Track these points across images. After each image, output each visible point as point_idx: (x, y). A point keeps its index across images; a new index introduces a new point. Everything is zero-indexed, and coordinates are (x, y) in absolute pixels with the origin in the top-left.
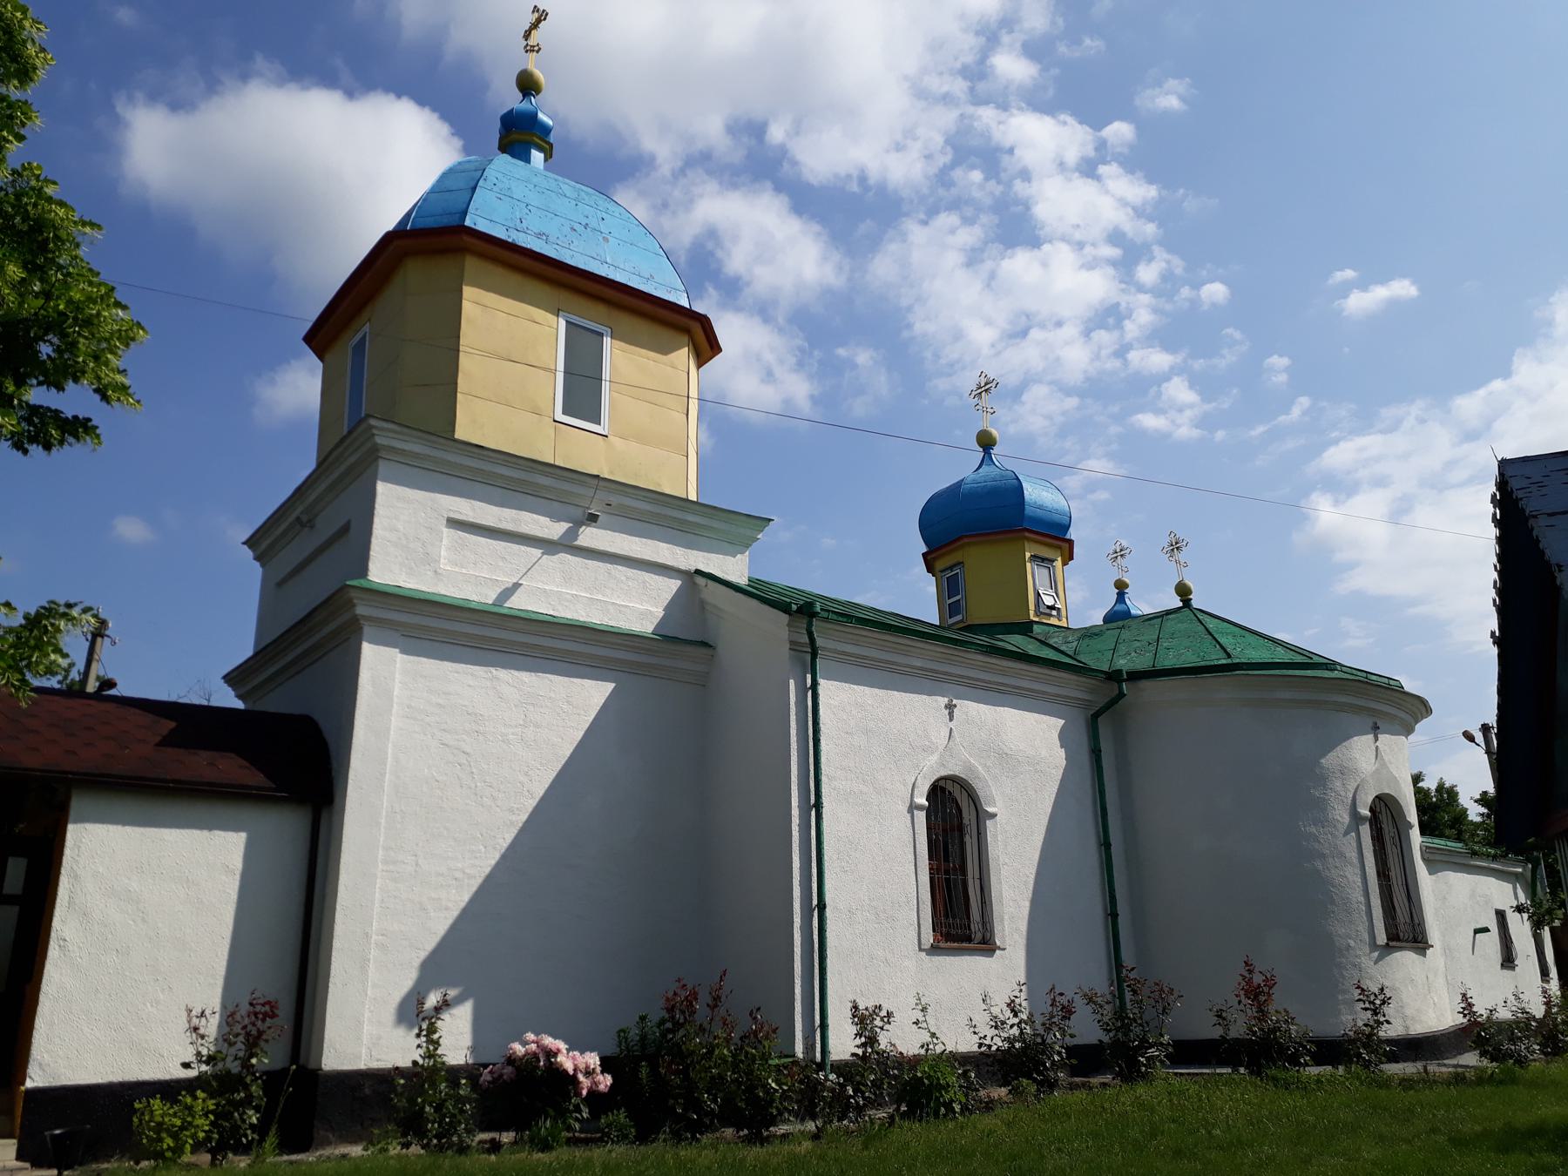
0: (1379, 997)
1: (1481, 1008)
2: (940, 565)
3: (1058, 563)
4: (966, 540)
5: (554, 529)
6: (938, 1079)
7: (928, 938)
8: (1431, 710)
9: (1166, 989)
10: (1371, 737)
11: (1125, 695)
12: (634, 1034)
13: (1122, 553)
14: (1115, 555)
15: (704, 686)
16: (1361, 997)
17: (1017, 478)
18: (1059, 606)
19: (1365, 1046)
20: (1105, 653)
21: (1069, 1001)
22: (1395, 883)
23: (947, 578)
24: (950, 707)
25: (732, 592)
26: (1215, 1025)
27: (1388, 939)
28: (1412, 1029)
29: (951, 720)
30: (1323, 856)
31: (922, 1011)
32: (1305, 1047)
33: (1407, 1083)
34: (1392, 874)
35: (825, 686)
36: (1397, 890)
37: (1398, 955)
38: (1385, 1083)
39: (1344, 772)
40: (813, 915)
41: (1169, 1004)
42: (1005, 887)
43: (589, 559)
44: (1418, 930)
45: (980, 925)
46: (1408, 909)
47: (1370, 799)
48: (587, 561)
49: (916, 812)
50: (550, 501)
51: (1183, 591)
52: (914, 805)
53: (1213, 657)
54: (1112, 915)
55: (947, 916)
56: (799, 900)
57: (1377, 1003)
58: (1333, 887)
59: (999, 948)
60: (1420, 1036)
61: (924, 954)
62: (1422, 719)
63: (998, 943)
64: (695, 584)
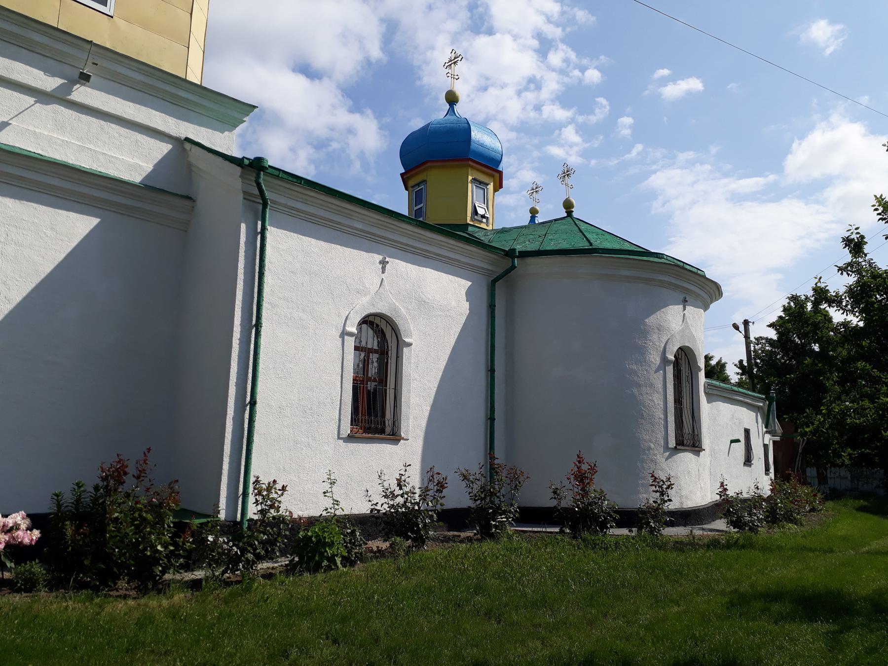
0: (666, 483)
1: (731, 493)
2: (411, 183)
3: (491, 187)
4: (429, 164)
5: (50, 83)
6: (325, 538)
7: (346, 429)
8: (722, 294)
9: (518, 472)
10: (681, 306)
11: (516, 267)
12: (68, 498)
13: (537, 190)
14: (532, 191)
15: (186, 231)
16: (654, 483)
17: (468, 123)
18: (488, 216)
19: (653, 517)
20: (509, 241)
21: (443, 478)
22: (685, 406)
23: (416, 192)
24: (384, 263)
25: (206, 152)
26: (552, 498)
27: (676, 444)
28: (685, 504)
29: (383, 272)
30: (639, 385)
31: (331, 483)
32: (611, 516)
33: (679, 546)
34: (684, 401)
35: (273, 234)
36: (686, 412)
37: (682, 455)
38: (663, 546)
39: (660, 328)
40: (246, 409)
41: (520, 483)
42: (412, 395)
43: (83, 114)
44: (696, 438)
45: (390, 421)
46: (692, 425)
47: (676, 349)
48: (80, 115)
49: (346, 337)
50: (45, 58)
51: (568, 206)
52: (345, 332)
53: (580, 245)
54: (491, 419)
55: (370, 415)
56: (234, 397)
57: (663, 487)
58: (644, 407)
59: (403, 439)
60: (689, 509)
61: (341, 441)
62: (715, 301)
63: (403, 435)
64: (184, 150)
